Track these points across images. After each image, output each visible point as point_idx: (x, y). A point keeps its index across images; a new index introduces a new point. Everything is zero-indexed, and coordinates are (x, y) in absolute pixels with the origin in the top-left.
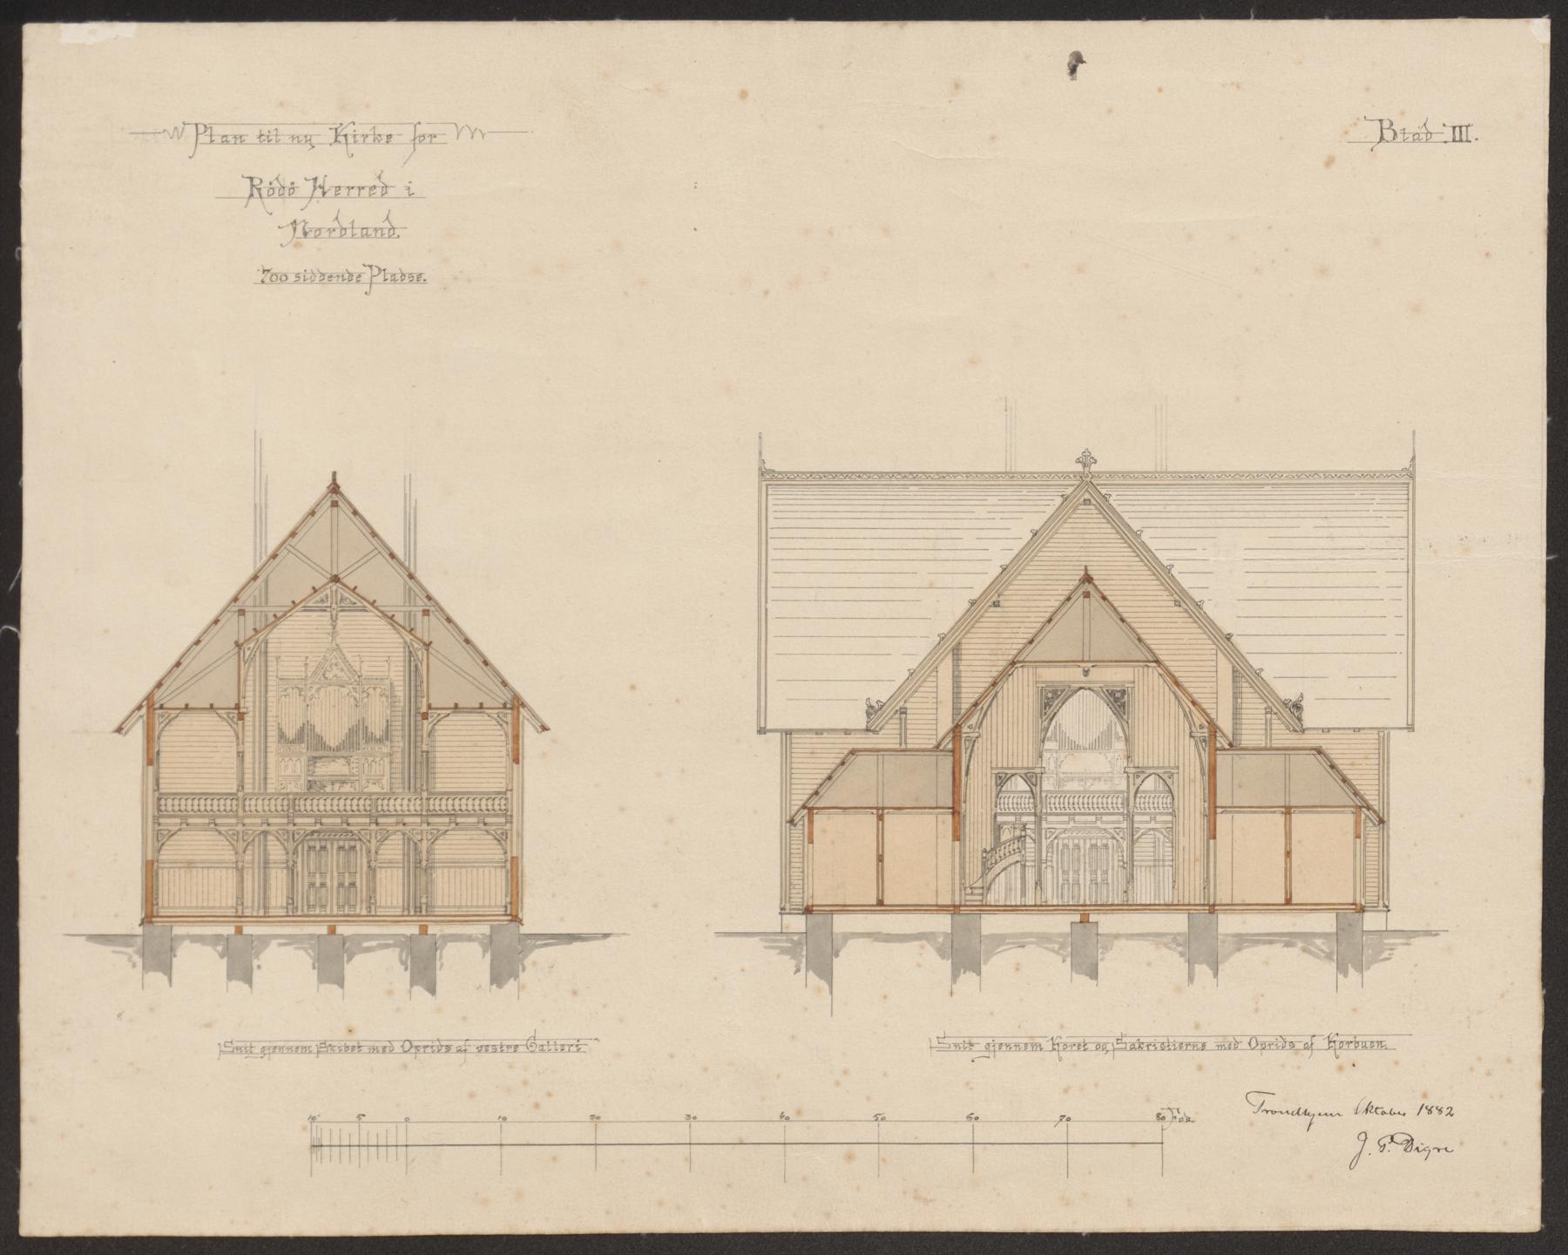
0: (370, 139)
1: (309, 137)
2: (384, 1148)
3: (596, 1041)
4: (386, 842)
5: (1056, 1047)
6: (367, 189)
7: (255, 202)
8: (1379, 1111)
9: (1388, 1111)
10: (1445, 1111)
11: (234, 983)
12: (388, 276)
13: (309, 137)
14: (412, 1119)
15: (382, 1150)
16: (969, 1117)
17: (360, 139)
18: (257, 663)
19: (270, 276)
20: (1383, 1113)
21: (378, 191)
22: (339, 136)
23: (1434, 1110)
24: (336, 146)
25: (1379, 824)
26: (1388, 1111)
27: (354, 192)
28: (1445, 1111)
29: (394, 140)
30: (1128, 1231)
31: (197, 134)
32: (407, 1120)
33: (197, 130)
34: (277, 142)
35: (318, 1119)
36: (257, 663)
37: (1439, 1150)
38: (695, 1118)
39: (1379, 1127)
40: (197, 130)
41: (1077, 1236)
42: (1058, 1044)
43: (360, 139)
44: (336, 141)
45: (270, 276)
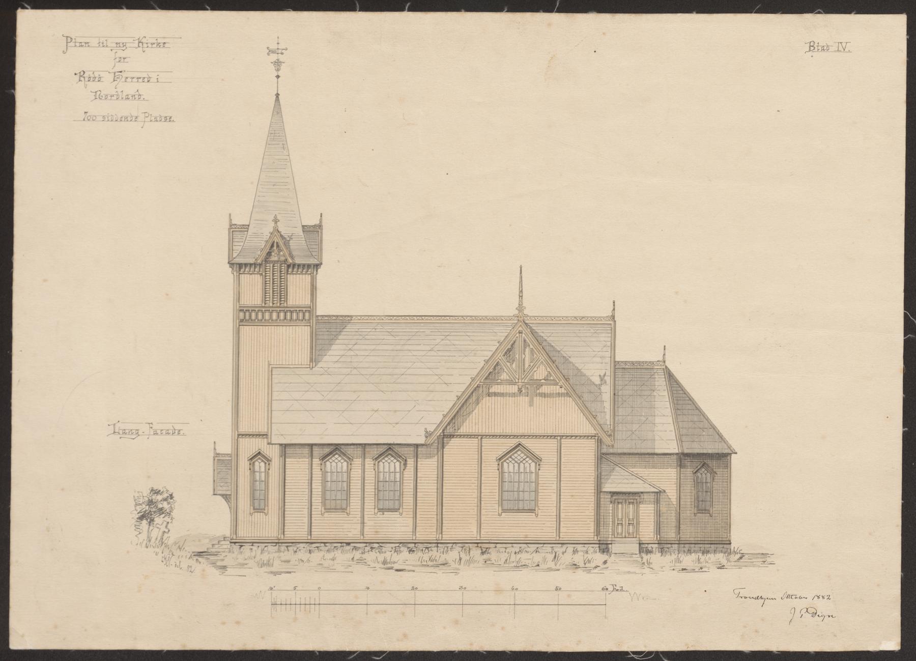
1: (124, 44)
4: (582, 414)
8: (793, 597)
9: (798, 596)
10: (826, 597)
11: (738, 539)
12: (153, 118)
13: (124, 44)
15: (308, 606)
16: (603, 589)
18: (535, 351)
19: (88, 117)
23: (821, 597)
26: (798, 596)
28: (826, 597)
31: (67, 43)
32: (319, 588)
33: (67, 40)
35: (274, 589)
36: (535, 351)
37: (829, 616)
38: (465, 588)
39: (800, 604)
40: (67, 40)
41: (903, 505)
45: (88, 117)
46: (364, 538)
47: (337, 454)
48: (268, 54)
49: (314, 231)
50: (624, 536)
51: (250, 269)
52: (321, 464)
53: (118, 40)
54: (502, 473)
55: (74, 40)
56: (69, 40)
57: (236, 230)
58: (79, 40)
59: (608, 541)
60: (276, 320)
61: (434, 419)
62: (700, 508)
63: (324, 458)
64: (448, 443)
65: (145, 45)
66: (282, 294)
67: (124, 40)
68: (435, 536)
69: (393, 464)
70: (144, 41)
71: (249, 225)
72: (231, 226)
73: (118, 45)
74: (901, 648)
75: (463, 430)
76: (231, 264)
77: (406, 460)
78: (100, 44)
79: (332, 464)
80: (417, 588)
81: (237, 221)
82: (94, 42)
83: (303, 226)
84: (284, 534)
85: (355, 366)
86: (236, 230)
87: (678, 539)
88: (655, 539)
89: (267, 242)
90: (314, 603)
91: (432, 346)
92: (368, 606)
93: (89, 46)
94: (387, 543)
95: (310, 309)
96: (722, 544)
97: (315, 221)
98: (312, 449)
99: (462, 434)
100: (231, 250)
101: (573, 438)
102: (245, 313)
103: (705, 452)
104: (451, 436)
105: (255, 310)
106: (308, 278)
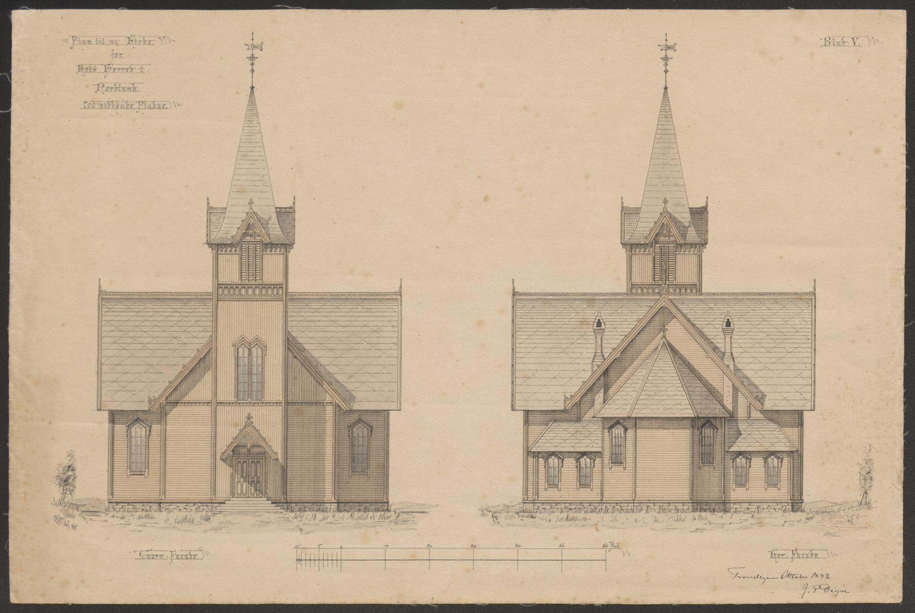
0: (142, 43)
2: (325, 559)
3: (744, 577)
5: (773, 556)
6: (125, 70)
7: (80, 73)
8: (794, 576)
9: (798, 576)
10: (825, 576)
11: (395, 497)
14: (344, 547)
17: (138, 43)
20: (796, 577)
21: (129, 70)
22: (130, 40)
24: (129, 45)
25: (779, 414)
27: (121, 71)
29: (151, 43)
30: (564, 603)
32: (341, 548)
34: (104, 43)
42: (775, 554)
43: (138, 43)
44: (129, 43)
46: (216, 499)
47: (360, 423)
48: (675, 44)
49: (286, 214)
50: (247, 496)
51: (695, 250)
52: (349, 431)
53: (112, 39)
54: (352, 438)
55: (78, 39)
56: (75, 38)
57: (628, 213)
58: (82, 39)
59: (730, 500)
60: (238, 295)
61: (158, 389)
62: (134, 469)
63: (612, 427)
64: (169, 412)
65: (134, 43)
66: (258, 270)
67: (116, 39)
68: (209, 496)
69: (134, 429)
70: (133, 38)
71: (640, 208)
72: (622, 208)
73: (89, 43)
74: (12, 604)
75: (190, 397)
76: (624, 245)
77: (151, 427)
78: (98, 42)
79: (137, 430)
80: (519, 546)
81: (630, 203)
82: (93, 41)
83: (689, 208)
84: (165, 495)
85: (175, 339)
86: (628, 213)
87: (633, 498)
88: (789, 498)
89: (655, 224)
90: (305, 559)
91: (129, 317)
92: (342, 561)
93: (91, 44)
94: (744, 502)
95: (282, 286)
96: (382, 505)
97: (286, 203)
98: (528, 414)
99: (228, 401)
100: (623, 232)
101: (205, 404)
102: (229, 290)
103: (674, 416)
104: (176, 403)
105: (245, 287)
106: (694, 259)
